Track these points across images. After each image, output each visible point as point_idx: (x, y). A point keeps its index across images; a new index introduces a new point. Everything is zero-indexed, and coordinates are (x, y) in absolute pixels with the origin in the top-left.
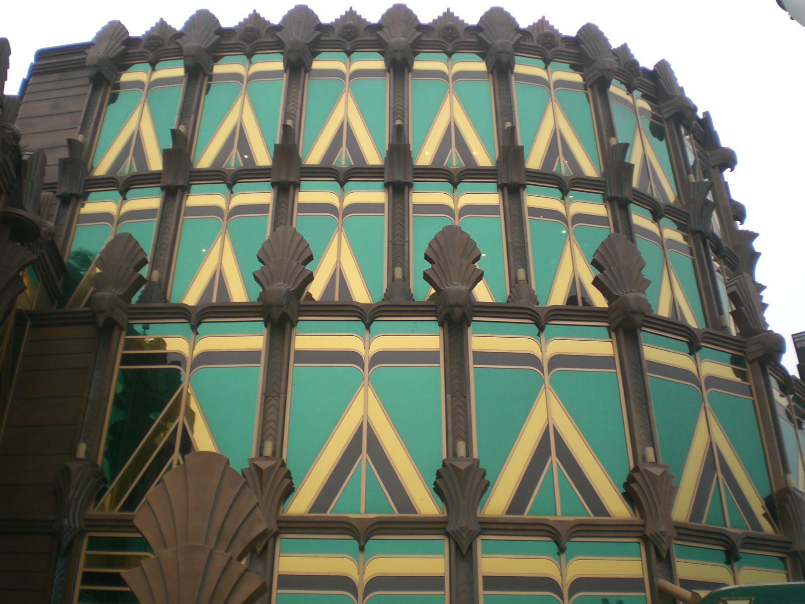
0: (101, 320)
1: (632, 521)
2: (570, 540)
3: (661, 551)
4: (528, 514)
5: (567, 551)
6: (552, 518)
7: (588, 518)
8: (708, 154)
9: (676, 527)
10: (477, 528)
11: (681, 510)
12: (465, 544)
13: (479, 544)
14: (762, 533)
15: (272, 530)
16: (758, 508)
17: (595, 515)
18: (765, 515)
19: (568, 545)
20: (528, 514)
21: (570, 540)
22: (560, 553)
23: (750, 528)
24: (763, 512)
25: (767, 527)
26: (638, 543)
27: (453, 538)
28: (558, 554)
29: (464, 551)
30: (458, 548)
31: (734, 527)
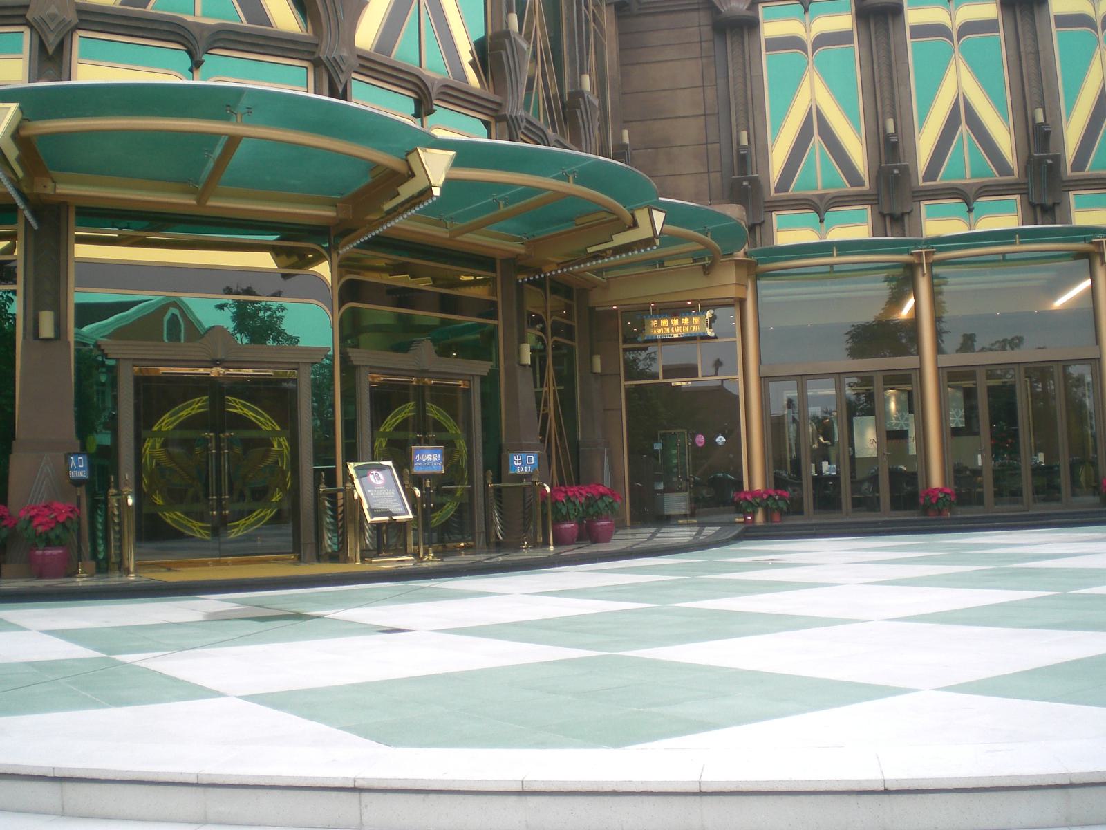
0: (1008, 347)
1: (299, 36)
2: (209, 52)
3: (337, 82)
4: (941, 179)
5: (203, 67)
6: (189, 18)
7: (240, 24)
8: (451, 536)
9: (360, 57)
10: (73, 17)
11: (366, 35)
12: (52, 41)
13: (78, 42)
14: (270, 28)
15: (70, 21)
16: (466, 56)
17: (248, 23)
18: (472, 64)
19: (205, 57)
20: (940, 181)
21: (209, 52)
22: (194, 69)
23: (848, 185)
24: (471, 58)
25: (473, 79)
26: (306, 68)
27: (36, 30)
28: (191, 70)
29: (51, 50)
30: (42, 46)
31: (434, 67)
